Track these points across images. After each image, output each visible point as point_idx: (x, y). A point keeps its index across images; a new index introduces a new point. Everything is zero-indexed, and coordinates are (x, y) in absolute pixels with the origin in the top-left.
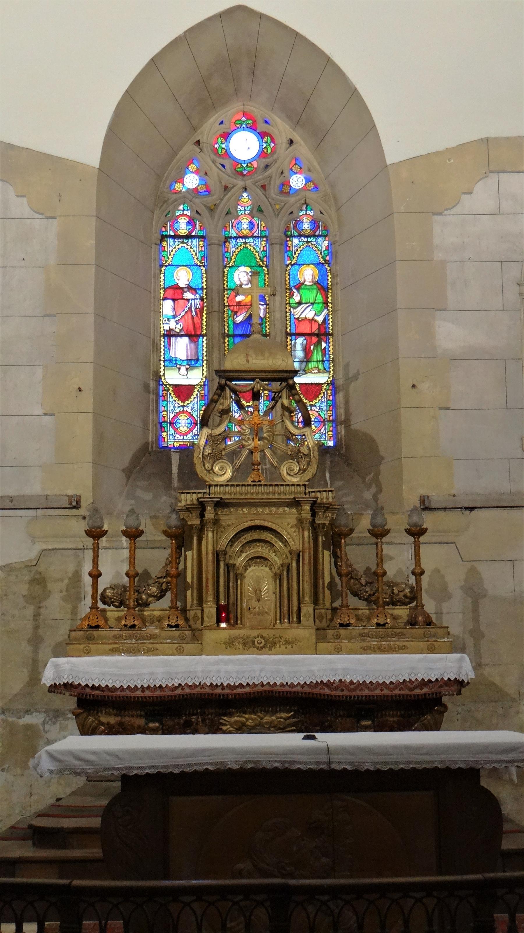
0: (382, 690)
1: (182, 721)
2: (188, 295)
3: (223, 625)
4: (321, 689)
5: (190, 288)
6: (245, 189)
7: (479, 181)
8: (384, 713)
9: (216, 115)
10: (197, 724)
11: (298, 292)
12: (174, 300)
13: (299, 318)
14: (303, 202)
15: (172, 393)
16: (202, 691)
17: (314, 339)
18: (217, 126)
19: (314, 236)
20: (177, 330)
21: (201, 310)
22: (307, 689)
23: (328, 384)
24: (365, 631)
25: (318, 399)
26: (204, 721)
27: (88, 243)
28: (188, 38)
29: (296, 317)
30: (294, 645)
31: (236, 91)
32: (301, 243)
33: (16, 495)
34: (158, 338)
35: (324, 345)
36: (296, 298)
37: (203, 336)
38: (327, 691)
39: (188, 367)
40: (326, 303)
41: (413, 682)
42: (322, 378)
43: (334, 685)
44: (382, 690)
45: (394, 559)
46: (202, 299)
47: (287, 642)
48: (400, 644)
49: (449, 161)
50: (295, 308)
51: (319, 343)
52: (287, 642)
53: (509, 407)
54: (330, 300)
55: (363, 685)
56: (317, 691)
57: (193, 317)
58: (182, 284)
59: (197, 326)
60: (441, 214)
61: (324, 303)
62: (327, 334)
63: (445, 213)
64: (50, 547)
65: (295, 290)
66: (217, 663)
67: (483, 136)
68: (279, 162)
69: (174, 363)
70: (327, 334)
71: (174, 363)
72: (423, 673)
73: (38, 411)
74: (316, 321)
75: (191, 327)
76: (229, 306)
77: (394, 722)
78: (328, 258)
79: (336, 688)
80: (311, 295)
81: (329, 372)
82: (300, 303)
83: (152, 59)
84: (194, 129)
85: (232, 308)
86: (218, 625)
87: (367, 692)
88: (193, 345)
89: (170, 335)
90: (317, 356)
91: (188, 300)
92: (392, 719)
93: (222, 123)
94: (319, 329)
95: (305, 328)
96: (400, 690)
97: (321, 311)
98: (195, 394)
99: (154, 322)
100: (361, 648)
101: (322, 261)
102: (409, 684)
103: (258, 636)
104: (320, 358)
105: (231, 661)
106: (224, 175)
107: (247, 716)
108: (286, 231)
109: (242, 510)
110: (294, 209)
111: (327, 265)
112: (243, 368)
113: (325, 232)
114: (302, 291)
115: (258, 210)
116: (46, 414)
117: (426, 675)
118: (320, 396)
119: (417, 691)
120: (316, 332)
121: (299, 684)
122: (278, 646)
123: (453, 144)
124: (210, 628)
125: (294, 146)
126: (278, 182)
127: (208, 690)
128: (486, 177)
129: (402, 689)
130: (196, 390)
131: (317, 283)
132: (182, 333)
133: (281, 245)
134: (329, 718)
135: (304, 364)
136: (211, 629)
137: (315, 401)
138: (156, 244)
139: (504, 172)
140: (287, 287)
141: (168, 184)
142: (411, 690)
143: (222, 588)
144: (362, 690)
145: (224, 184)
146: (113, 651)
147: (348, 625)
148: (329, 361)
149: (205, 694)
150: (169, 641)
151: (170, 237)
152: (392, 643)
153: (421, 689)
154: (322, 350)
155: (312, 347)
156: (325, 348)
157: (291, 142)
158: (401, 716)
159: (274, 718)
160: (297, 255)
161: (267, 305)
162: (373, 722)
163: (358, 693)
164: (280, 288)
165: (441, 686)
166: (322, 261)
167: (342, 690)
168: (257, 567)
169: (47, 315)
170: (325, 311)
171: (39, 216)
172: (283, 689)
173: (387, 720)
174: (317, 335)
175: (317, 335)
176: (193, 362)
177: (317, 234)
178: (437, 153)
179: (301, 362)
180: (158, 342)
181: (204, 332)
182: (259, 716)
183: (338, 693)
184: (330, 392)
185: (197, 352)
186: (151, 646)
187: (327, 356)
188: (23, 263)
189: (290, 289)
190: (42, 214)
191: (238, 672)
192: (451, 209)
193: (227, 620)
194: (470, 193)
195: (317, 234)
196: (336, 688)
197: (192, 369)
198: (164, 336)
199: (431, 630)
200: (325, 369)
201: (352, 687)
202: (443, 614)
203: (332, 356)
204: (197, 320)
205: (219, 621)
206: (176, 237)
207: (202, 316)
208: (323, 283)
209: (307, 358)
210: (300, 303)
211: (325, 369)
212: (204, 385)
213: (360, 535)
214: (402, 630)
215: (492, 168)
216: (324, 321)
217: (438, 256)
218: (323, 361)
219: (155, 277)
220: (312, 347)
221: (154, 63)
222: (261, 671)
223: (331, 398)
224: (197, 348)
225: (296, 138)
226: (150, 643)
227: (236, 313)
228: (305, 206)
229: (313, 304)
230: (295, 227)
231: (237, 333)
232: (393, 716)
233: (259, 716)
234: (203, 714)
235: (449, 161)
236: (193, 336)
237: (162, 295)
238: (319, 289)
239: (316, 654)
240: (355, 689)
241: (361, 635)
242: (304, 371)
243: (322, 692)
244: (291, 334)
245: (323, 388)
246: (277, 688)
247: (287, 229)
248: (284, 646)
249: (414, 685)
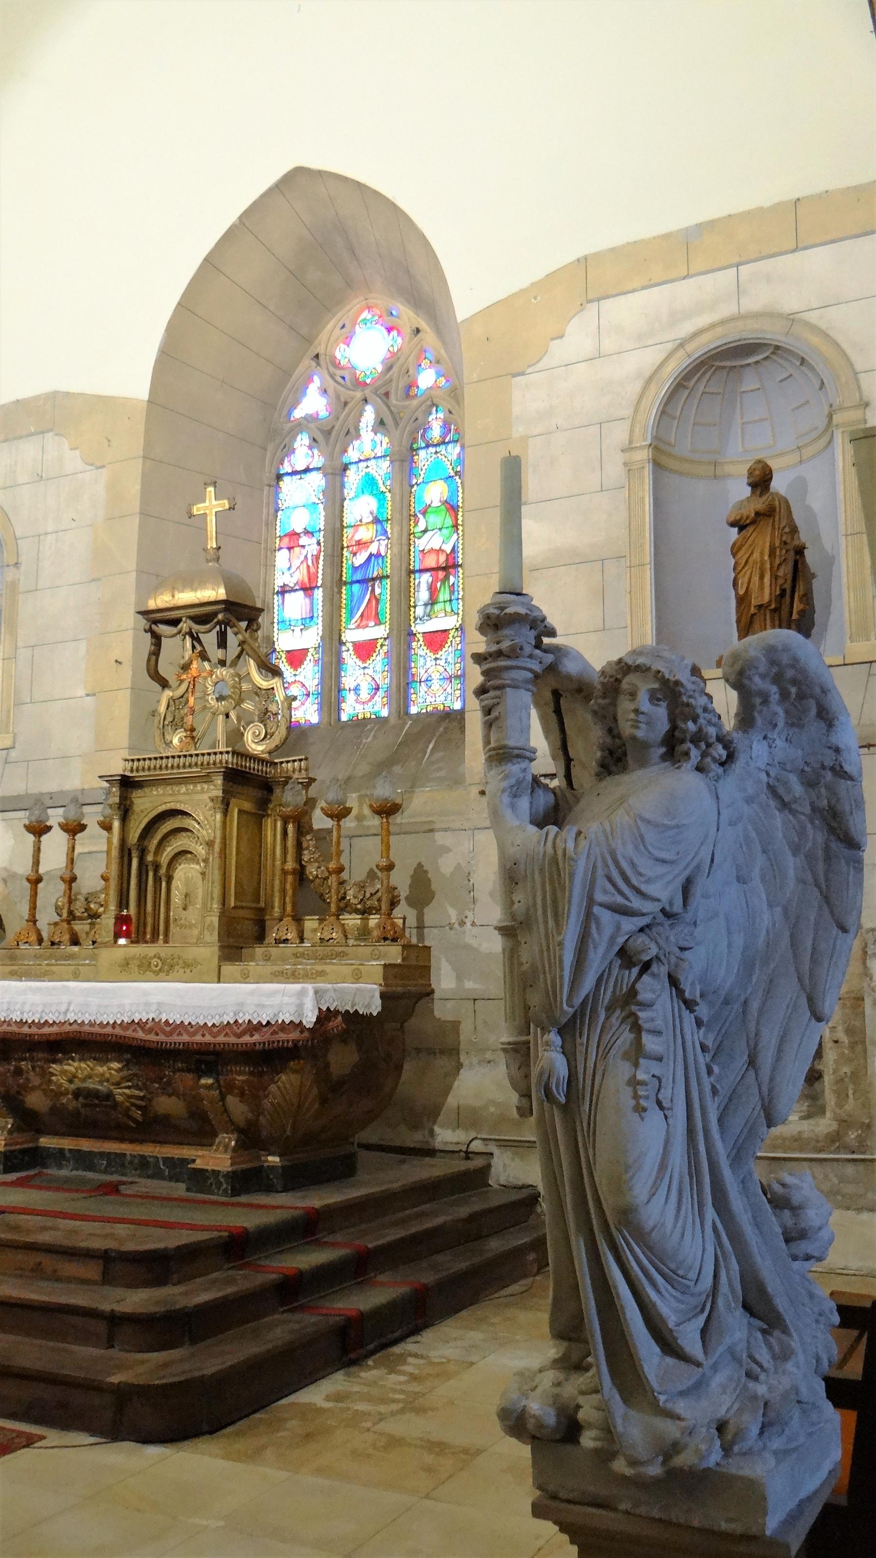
0: (203, 1035)
1: (12, 1068)
2: (304, 540)
3: (122, 941)
4: (134, 1031)
5: (307, 532)
6: (366, 401)
7: (574, 316)
8: (229, 1068)
9: (334, 319)
10: (27, 1072)
11: (424, 517)
12: (290, 549)
13: (423, 550)
14: (429, 403)
15: (285, 661)
16: (10, 1029)
17: (441, 574)
18: (337, 331)
19: (443, 443)
20: (292, 585)
21: (317, 557)
22: (118, 1031)
23: (457, 629)
24: (300, 949)
25: (444, 650)
26: (33, 1068)
27: (134, 488)
28: (247, 224)
29: (421, 549)
30: (194, 970)
31: (349, 284)
32: (429, 456)
33: (55, 790)
34: (270, 596)
35: (452, 579)
36: (422, 525)
37: (318, 587)
38: (140, 1035)
39: (302, 627)
40: (455, 526)
41: (241, 1025)
42: (449, 622)
43: (148, 1026)
44: (203, 1035)
45: (451, 850)
46: (319, 543)
47: (187, 965)
48: (319, 968)
49: (535, 298)
50: (419, 538)
51: (447, 578)
52: (187, 965)
53: (607, 626)
54: (460, 522)
55: (181, 1027)
56: (129, 1033)
57: (308, 567)
58: (299, 530)
59: (312, 577)
60: (522, 374)
61: (453, 526)
62: (456, 566)
63: (529, 370)
64: (86, 850)
65: (420, 516)
66: (252, 993)
67: (580, 254)
68: (402, 360)
69: (288, 625)
70: (456, 566)
71: (288, 625)
72: (251, 1012)
73: (81, 692)
74: (443, 551)
75: (306, 580)
76: (348, 547)
77: (243, 1082)
78: (459, 469)
79: (150, 1031)
80: (440, 518)
81: (458, 614)
82: (425, 531)
83: (205, 259)
84: (309, 340)
85: (351, 549)
86: (116, 942)
87: (185, 1038)
88: (307, 601)
89: (284, 591)
90: (444, 595)
91: (303, 547)
92: (240, 1078)
93: (343, 327)
94: (447, 560)
95: (431, 562)
96: (225, 1036)
97: (450, 537)
98: (308, 659)
99: (265, 578)
100: (271, 974)
101: (452, 474)
102: (235, 1028)
103: (155, 956)
104: (447, 597)
105: (39, 990)
106: (342, 389)
107: (76, 1064)
108: (412, 444)
109: (172, 789)
110: (419, 414)
111: (457, 477)
112: (168, 605)
113: (456, 438)
114: (427, 515)
115: (380, 424)
116: (88, 695)
117: (255, 1015)
118: (447, 646)
119: (247, 1039)
120: (444, 565)
121: (108, 1023)
122: (176, 970)
123: (540, 275)
124: (105, 945)
125: (419, 335)
126: (402, 384)
127: (14, 1028)
128: (582, 310)
129: (226, 1035)
130: (309, 654)
131: (445, 503)
132: (297, 587)
133: (403, 461)
134: (167, 1073)
135: (429, 607)
136: (106, 947)
137: (440, 653)
138: (270, 486)
139: (608, 297)
140: (412, 513)
141: (285, 412)
142: (239, 1036)
143: (549, 902)
144: (180, 1034)
145: (343, 400)
146: (276, 976)
147: (286, 941)
148: (458, 599)
149: (73, 1032)
150: (87, 962)
151: (288, 474)
152: (309, 967)
153: (252, 1036)
154: (449, 587)
155: (439, 584)
156: (453, 584)
157: (418, 331)
158: (251, 1073)
159: (105, 1068)
160: (424, 471)
161: (389, 539)
162: (217, 1081)
163: (175, 1038)
164: (404, 515)
165: (274, 1033)
166: (452, 474)
167: (157, 1034)
168: (187, 865)
169: (93, 580)
170: (455, 536)
171: (90, 468)
172: (92, 1030)
173: (234, 1079)
174: (444, 569)
175: (444, 569)
176: (308, 621)
177: (447, 440)
178: (522, 292)
179: (426, 605)
180: (271, 601)
181: (319, 584)
182: (88, 1066)
183: (152, 1037)
184: (458, 639)
185: (312, 610)
186: (48, 968)
187: (456, 593)
188: (74, 524)
189: (415, 515)
190: (92, 465)
191: (45, 1005)
192: (535, 364)
193: (127, 935)
194: (561, 337)
195: (447, 440)
196: (150, 1031)
197: (307, 629)
198: (278, 593)
199: (381, 948)
200: (452, 611)
201: (168, 1029)
202: (416, 925)
203: (461, 593)
204: (312, 570)
205: (117, 935)
206: (294, 473)
207: (318, 563)
208: (453, 500)
209: (433, 601)
210: (425, 531)
211: (452, 611)
212: (319, 647)
213: (412, 820)
214: (340, 949)
215: (590, 297)
216: (453, 550)
217: (518, 431)
218: (451, 600)
219: (267, 524)
220: (439, 584)
221: (211, 264)
222: (69, 1004)
223: (459, 647)
224: (312, 604)
225: (423, 325)
226: (47, 965)
227: (355, 554)
228: (434, 409)
229: (440, 529)
230: (423, 436)
231: (355, 579)
232: (240, 1073)
233: (88, 1066)
234: (32, 1059)
235: (535, 298)
236: (307, 589)
237: (277, 545)
238: (448, 510)
239: (219, 982)
240: (171, 1034)
241: (295, 955)
242: (429, 615)
243: (134, 1035)
244: (414, 572)
245: (450, 636)
246: (87, 1029)
247: (415, 440)
248: (183, 970)
249: (241, 1029)
